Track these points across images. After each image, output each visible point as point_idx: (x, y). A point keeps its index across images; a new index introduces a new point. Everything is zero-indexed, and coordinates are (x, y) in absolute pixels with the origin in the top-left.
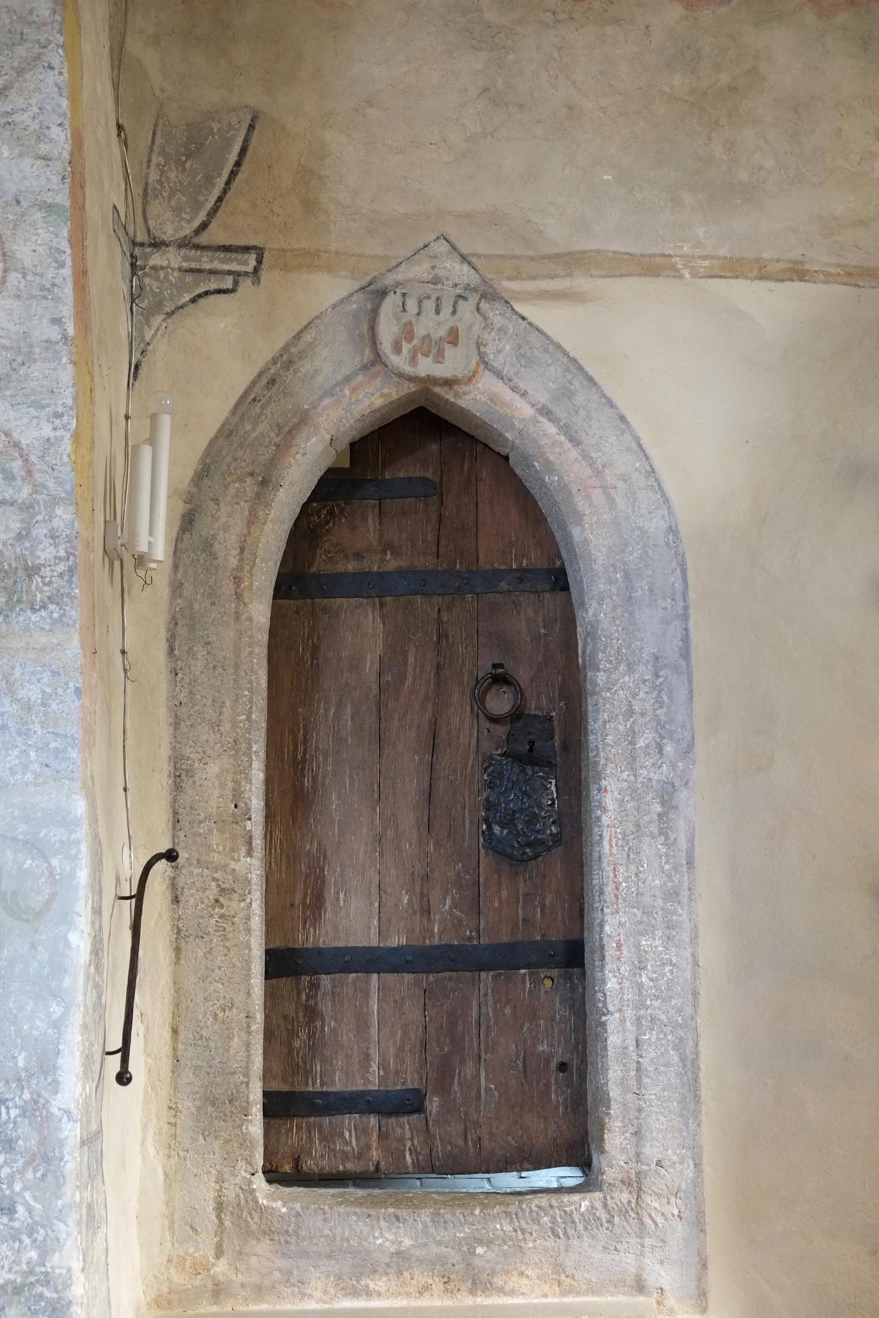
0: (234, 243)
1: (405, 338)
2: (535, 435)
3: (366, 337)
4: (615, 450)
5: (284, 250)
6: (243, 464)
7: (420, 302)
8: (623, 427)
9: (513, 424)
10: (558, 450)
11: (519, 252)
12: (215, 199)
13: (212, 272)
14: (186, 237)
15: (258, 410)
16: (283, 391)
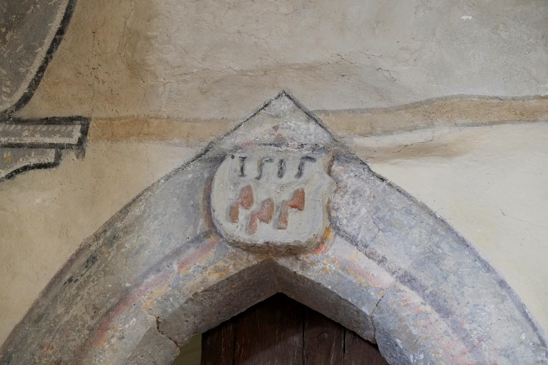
0: (58, 115)
1: (242, 204)
2: (395, 306)
3: (201, 208)
4: (494, 321)
5: (111, 119)
6: (50, 352)
7: (261, 166)
8: (504, 292)
9: (369, 294)
10: (422, 322)
11: (372, 104)
12: (36, 69)
13: (33, 146)
14: (6, 111)
15: (73, 291)
16: (103, 270)
